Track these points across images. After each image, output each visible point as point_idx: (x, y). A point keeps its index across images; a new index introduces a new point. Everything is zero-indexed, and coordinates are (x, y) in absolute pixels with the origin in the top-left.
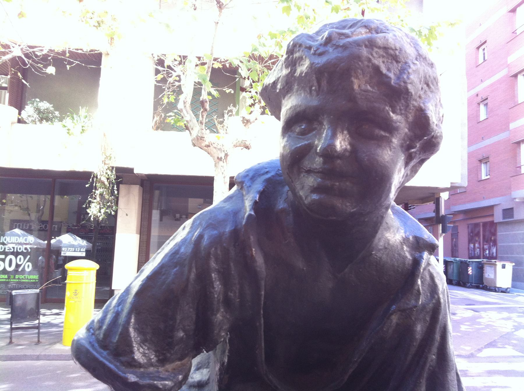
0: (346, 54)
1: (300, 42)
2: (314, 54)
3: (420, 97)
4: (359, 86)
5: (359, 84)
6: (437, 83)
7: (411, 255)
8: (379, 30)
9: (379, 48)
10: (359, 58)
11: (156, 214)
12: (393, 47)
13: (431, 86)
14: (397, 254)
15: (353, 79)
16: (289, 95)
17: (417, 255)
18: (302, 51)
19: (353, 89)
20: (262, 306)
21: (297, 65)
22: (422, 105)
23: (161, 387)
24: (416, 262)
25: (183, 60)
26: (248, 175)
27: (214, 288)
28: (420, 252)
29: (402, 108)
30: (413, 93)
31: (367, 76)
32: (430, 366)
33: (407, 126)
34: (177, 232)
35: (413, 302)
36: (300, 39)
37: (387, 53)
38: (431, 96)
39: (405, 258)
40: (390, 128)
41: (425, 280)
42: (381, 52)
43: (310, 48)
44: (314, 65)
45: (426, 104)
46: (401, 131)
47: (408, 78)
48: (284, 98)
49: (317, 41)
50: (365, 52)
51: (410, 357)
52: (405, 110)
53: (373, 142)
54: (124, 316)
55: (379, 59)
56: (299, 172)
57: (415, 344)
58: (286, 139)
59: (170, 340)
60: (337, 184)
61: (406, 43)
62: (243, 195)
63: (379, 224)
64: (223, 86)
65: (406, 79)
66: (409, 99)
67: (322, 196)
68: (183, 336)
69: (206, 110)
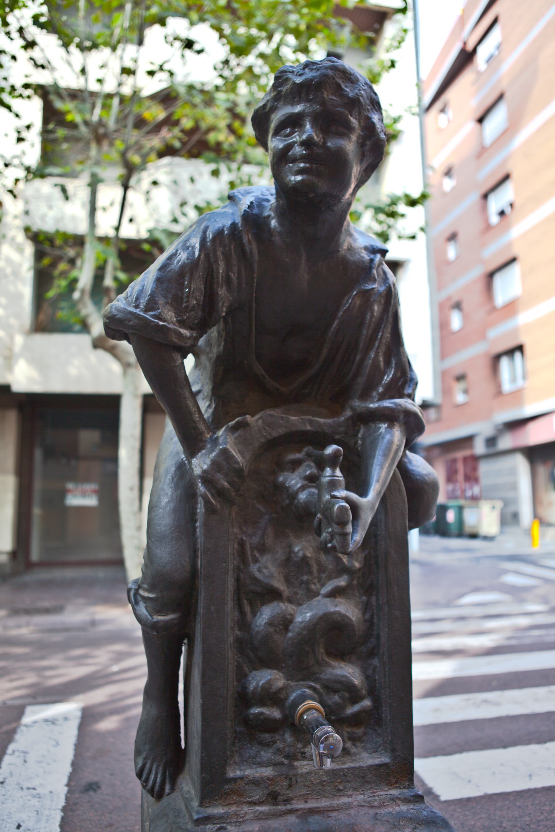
0: (319, 73)
11: (38, 454)
32: (386, 341)
40: (349, 128)
41: (380, 274)
46: (357, 131)
67: (304, 176)
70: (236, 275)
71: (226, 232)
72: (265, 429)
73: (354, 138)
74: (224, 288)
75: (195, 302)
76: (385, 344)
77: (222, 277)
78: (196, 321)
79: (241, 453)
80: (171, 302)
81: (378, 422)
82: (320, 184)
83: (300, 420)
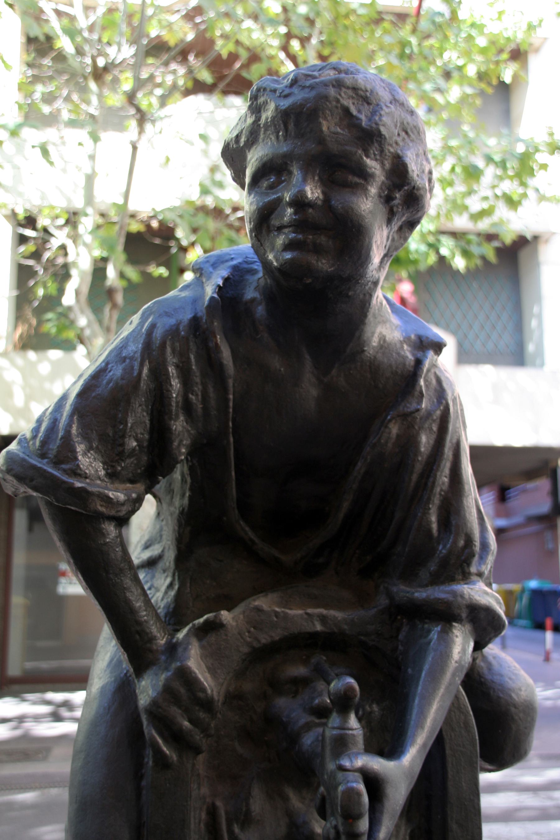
0: (313, 94)
1: (264, 85)
2: (280, 96)
3: (397, 143)
4: (328, 128)
5: (328, 126)
6: (419, 133)
7: (413, 355)
8: (350, 72)
9: (348, 88)
10: (326, 98)
12: (363, 88)
14: (396, 353)
15: (321, 120)
16: (255, 147)
17: (420, 354)
18: (267, 95)
19: (322, 131)
20: (231, 415)
21: (262, 111)
22: (399, 152)
24: (419, 363)
25: (72, 219)
26: (208, 262)
27: (171, 385)
28: (423, 352)
29: (376, 153)
30: (387, 136)
31: (336, 118)
32: (442, 490)
33: (384, 173)
34: (122, 329)
36: (264, 83)
37: (357, 94)
38: (411, 144)
40: (365, 175)
41: (430, 383)
42: (350, 92)
43: (275, 91)
44: (279, 107)
45: (404, 152)
46: (377, 179)
47: (381, 120)
48: (249, 151)
49: (282, 84)
50: (332, 92)
51: (415, 477)
52: (381, 156)
53: (347, 190)
54: (64, 419)
55: (348, 100)
56: (269, 231)
57: (420, 459)
58: (252, 196)
59: (121, 449)
60: (311, 237)
61: (379, 86)
62: (203, 283)
63: (368, 305)
64: (147, 263)
65: (378, 121)
66: (383, 142)
68: (135, 446)
69: (114, 306)
70: (200, 397)
71: (183, 333)
73: (373, 190)
74: (182, 418)
75: (135, 444)
76: (440, 494)
77: (177, 403)
78: (139, 471)
79: (212, 670)
80: (97, 447)
81: (427, 621)
82: (320, 264)
83: (305, 616)
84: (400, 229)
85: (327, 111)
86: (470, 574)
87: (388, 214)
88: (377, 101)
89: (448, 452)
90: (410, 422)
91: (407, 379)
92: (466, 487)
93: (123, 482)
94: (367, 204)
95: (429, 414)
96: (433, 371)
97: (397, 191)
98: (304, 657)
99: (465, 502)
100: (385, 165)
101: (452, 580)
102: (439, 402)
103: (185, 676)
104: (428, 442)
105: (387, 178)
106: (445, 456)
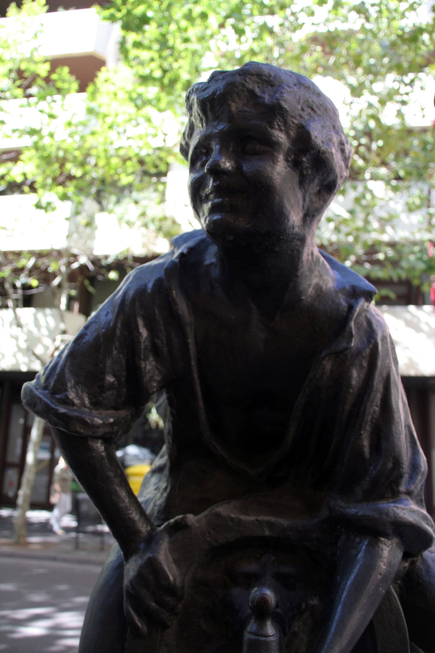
0: (224, 82)
7: (347, 302)
12: (267, 74)
13: (318, 111)
23: (89, 421)
24: (351, 308)
29: (280, 124)
30: (288, 109)
32: (373, 418)
35: (344, 344)
37: (261, 79)
38: (316, 118)
39: (339, 304)
40: (272, 145)
42: (254, 78)
52: (285, 126)
57: (351, 391)
66: (285, 115)
68: (114, 381)
72: (209, 533)
74: (151, 359)
76: (372, 422)
84: (319, 193)
85: (235, 95)
86: (399, 493)
87: (299, 177)
88: (280, 83)
89: (378, 384)
90: (343, 359)
91: (339, 322)
92: (396, 415)
93: (107, 409)
94: (279, 170)
95: (359, 352)
96: (364, 314)
97: (303, 156)
98: (258, 555)
99: (394, 429)
100: (290, 134)
101: (382, 497)
102: (369, 341)
103: (153, 566)
104: (359, 376)
105: (293, 145)
106: (374, 389)
